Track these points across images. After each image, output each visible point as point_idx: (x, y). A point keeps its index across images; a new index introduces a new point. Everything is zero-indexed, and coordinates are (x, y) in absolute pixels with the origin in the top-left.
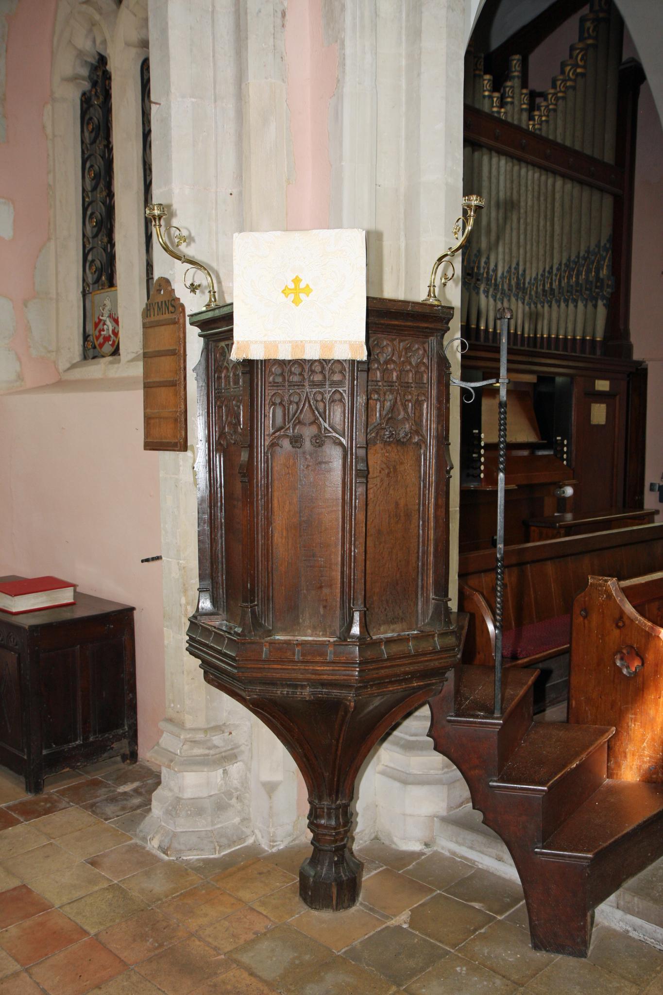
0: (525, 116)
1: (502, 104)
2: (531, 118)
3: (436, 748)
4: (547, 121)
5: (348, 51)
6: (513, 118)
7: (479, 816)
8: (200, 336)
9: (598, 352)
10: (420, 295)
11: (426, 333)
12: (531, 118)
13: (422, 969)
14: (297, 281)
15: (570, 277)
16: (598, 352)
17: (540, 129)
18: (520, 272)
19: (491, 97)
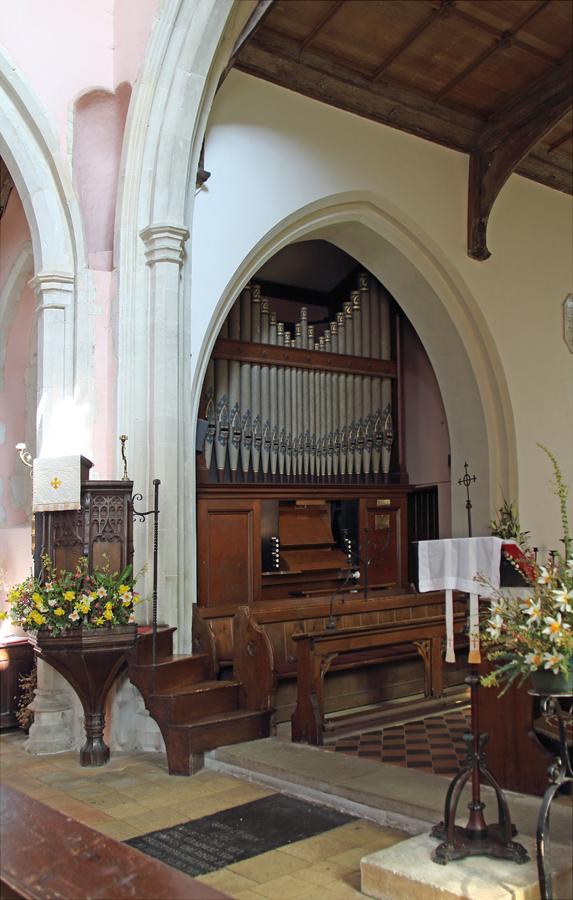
0: (311, 341)
1: (293, 337)
2: (316, 341)
3: (151, 715)
4: (330, 342)
5: (120, 361)
6: (301, 345)
7: (148, 712)
8: (13, 624)
9: (386, 481)
10: (119, 478)
11: (123, 494)
12: (316, 341)
13: (41, 613)
14: (56, 479)
15: (371, 428)
16: (386, 481)
17: (324, 348)
18: (311, 435)
19: (284, 336)
